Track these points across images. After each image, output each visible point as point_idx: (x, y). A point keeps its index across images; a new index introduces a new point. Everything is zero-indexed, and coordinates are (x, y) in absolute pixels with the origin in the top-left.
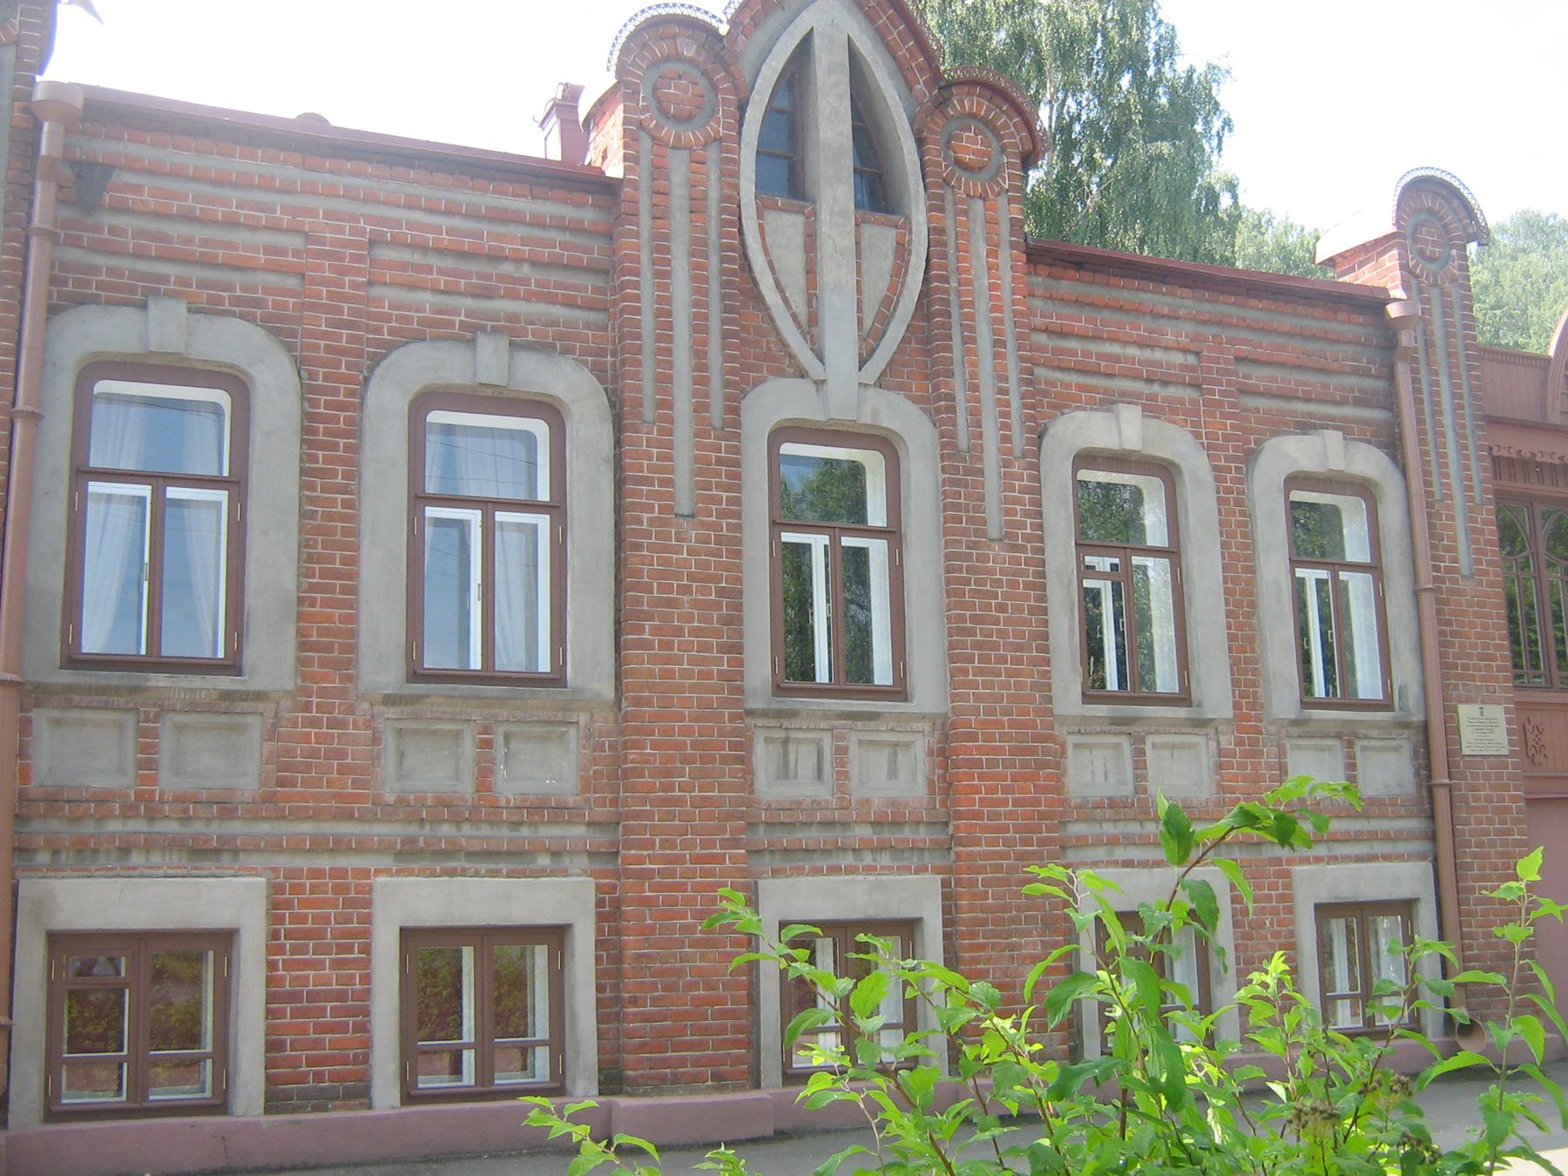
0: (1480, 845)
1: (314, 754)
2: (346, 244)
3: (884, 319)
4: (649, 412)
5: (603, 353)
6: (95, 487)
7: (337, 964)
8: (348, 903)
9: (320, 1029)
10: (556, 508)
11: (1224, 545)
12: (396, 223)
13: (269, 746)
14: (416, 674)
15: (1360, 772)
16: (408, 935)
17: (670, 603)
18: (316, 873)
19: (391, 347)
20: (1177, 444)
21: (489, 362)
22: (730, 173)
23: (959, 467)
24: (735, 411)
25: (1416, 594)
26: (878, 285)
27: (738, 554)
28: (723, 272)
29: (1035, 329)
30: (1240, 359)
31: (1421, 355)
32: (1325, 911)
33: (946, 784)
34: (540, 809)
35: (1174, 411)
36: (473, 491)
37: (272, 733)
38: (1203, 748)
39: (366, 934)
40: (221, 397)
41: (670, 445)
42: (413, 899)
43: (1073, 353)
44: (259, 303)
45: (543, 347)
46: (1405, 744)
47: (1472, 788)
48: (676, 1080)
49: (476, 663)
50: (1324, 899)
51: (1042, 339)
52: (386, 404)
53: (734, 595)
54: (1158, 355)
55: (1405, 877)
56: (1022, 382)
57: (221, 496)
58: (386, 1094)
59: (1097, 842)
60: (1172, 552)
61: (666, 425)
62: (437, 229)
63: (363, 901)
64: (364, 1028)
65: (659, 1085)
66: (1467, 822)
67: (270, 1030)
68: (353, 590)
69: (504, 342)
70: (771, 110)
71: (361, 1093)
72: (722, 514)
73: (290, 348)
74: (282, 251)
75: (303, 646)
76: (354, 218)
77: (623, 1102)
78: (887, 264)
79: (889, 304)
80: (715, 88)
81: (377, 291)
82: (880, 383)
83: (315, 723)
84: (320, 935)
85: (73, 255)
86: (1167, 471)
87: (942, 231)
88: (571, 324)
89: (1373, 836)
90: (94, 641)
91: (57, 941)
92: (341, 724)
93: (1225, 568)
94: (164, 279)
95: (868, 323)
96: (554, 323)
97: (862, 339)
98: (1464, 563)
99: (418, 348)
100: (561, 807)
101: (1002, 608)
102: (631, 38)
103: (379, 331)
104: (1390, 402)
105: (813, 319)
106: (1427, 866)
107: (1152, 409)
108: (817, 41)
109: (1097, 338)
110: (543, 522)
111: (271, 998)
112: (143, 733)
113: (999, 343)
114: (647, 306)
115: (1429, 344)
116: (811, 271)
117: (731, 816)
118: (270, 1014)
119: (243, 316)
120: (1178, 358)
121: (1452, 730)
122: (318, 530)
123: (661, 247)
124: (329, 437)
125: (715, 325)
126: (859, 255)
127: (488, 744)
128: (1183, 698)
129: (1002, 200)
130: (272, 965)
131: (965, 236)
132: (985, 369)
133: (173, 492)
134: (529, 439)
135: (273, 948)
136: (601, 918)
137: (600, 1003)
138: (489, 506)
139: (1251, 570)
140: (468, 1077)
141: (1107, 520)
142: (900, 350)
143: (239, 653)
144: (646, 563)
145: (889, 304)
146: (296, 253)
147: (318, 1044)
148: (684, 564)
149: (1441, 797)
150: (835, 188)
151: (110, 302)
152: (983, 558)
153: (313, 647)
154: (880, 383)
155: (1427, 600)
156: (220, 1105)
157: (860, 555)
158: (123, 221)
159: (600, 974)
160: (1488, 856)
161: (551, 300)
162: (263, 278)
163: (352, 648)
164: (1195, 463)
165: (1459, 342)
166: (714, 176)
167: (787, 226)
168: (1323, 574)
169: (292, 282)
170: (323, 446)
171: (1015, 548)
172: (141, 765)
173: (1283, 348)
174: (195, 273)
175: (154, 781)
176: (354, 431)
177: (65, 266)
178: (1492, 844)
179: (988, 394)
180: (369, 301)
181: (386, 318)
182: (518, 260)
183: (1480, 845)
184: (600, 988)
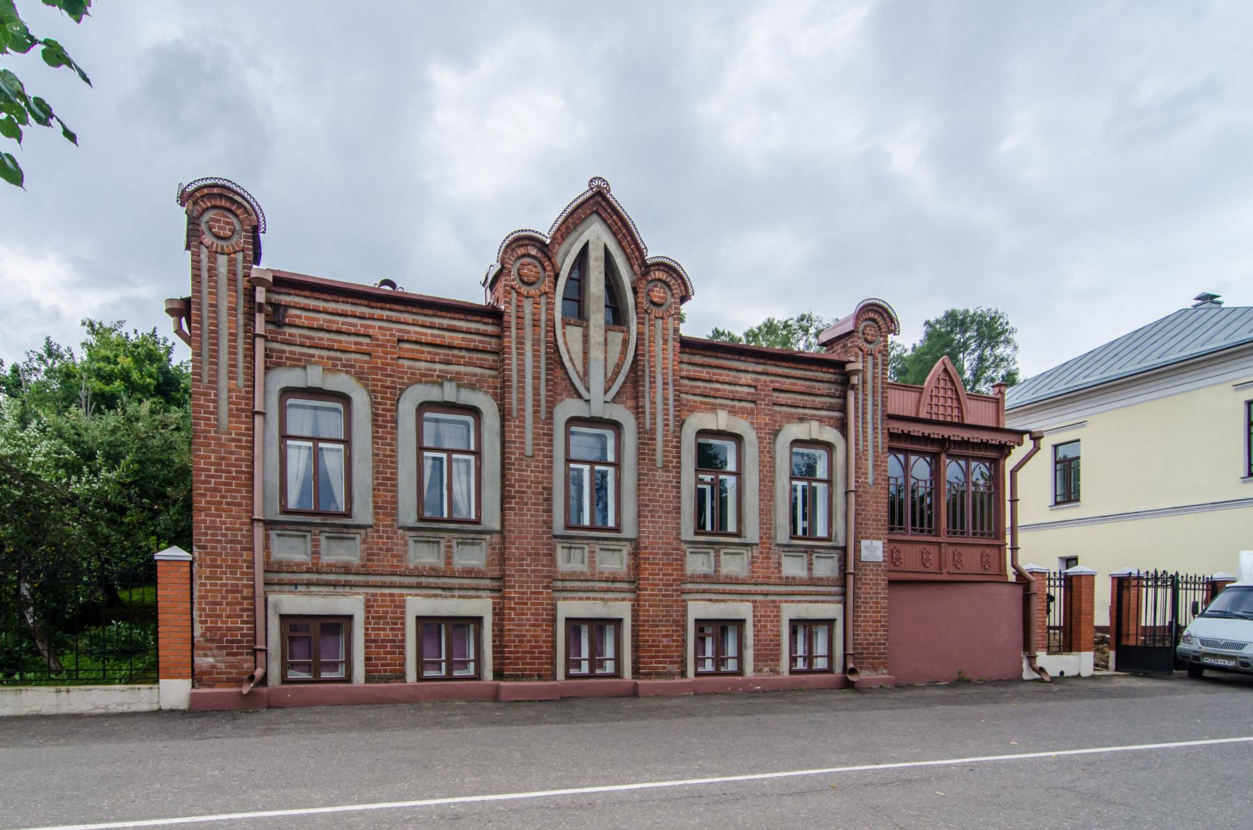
1: (381, 549)
2: (388, 341)
3: (616, 374)
4: (515, 414)
5: (496, 388)
6: (289, 442)
7: (391, 629)
8: (396, 606)
9: (385, 653)
10: (478, 453)
11: (761, 471)
12: (409, 332)
13: (364, 546)
14: (421, 519)
15: (814, 567)
16: (419, 619)
17: (523, 492)
18: (382, 595)
19: (408, 385)
20: (741, 426)
21: (449, 393)
22: (550, 307)
23: (645, 438)
24: (551, 413)
25: (847, 493)
26: (614, 356)
27: (551, 473)
28: (547, 353)
29: (682, 377)
30: (775, 390)
31: (860, 387)
32: (795, 624)
33: (636, 567)
34: (469, 573)
36: (446, 446)
37: (364, 541)
38: (746, 554)
39: (403, 618)
40: (339, 406)
41: (524, 427)
42: (418, 605)
43: (699, 387)
44: (353, 366)
45: (472, 387)
46: (836, 555)
48: (523, 676)
49: (445, 515)
50: (793, 617)
51: (686, 382)
52: (407, 408)
53: (549, 490)
54: (738, 388)
55: (832, 610)
56: (675, 400)
57: (341, 446)
58: (411, 676)
60: (738, 474)
61: (522, 418)
62: (426, 335)
63: (402, 606)
64: (402, 653)
65: (516, 677)
67: (366, 653)
68: (395, 485)
69: (454, 385)
70: (569, 278)
71: (401, 677)
72: (544, 456)
73: (366, 386)
74: (361, 344)
75: (376, 507)
76: (391, 329)
77: (502, 683)
78: (619, 348)
79: (618, 367)
80: (544, 269)
81: (401, 362)
82: (614, 400)
83: (381, 537)
84: (385, 618)
85: (275, 346)
86: (738, 438)
87: (643, 334)
88: (482, 375)
89: (817, 594)
90: (292, 503)
91: (283, 617)
92: (391, 538)
93: (760, 480)
94: (313, 356)
95: (609, 374)
96: (475, 375)
97: (606, 382)
98: (870, 479)
99: (416, 386)
100: (479, 571)
101: (661, 496)
102: (507, 247)
103: (402, 378)
104: (844, 409)
105: (586, 373)
106: (841, 606)
107: (733, 412)
108: (591, 246)
109: (710, 381)
110: (472, 458)
111: (366, 641)
112: (313, 540)
113: (665, 383)
114: (514, 367)
115: (864, 382)
116: (586, 353)
117: (546, 577)
118: (366, 647)
119: (346, 372)
120: (746, 389)
121: (857, 551)
122: (380, 461)
123: (520, 342)
124: (384, 422)
125: (543, 376)
126: (606, 344)
127: (450, 547)
128: (617, 529)
129: (671, 319)
130: (367, 629)
131: (653, 336)
132: (658, 396)
133: (321, 445)
134: (467, 424)
135: (367, 622)
136: (494, 614)
137: (494, 647)
138: (450, 452)
139: (773, 482)
140: (444, 673)
141: (707, 459)
142: (622, 387)
143: (350, 510)
144: (513, 475)
145: (618, 367)
146: (367, 345)
147: (385, 659)
148: (529, 476)
149: (851, 579)
150: (598, 316)
151: (291, 366)
152: (654, 475)
153: (380, 508)
154: (614, 400)
155: (852, 496)
156: (348, 679)
157: (604, 475)
158: (293, 331)
159: (494, 636)
161: (474, 365)
162: (353, 356)
163: (396, 509)
164: (750, 436)
166: (543, 309)
167: (575, 333)
168: (805, 483)
169: (366, 358)
170: (381, 427)
171: (668, 471)
172: (313, 553)
173: (795, 384)
174: (325, 353)
175: (319, 559)
176: (395, 421)
177: (272, 350)
179: (659, 406)
180: (399, 366)
181: (406, 373)
182: (460, 349)
184: (494, 641)
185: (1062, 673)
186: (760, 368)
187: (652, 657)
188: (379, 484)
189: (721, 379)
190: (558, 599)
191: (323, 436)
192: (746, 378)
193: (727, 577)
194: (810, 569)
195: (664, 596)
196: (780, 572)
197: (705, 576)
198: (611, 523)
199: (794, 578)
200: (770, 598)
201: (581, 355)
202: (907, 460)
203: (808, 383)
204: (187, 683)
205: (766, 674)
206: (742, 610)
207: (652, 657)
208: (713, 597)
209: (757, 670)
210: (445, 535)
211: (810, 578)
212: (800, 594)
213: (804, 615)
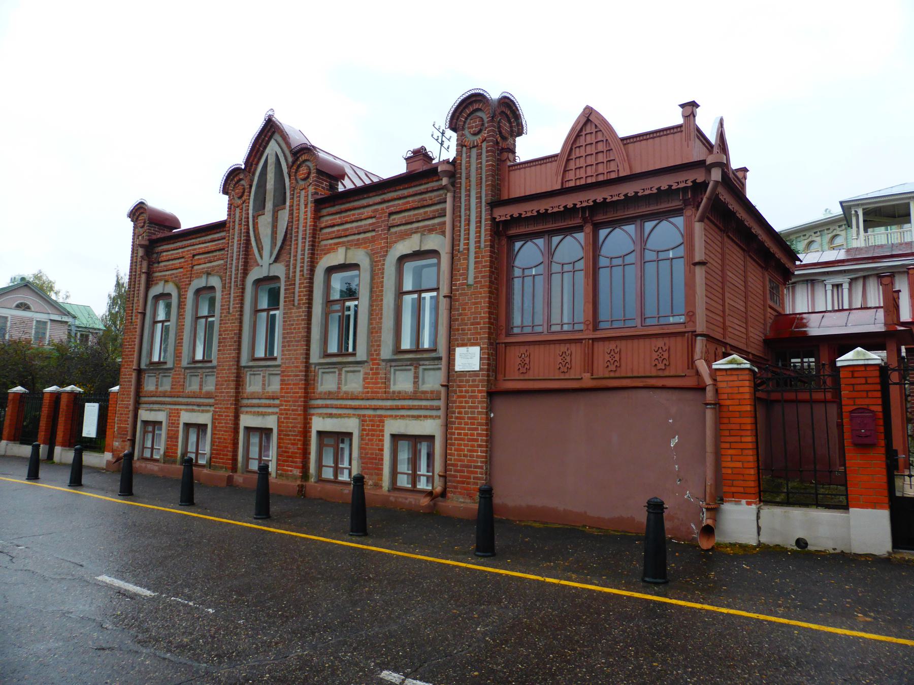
0: (460, 413)
35: (365, 243)
38: (362, 370)
47: (459, 386)
55: (430, 426)
66: (455, 402)
89: (420, 408)
109: (342, 224)
160: (463, 418)
178: (466, 413)
183: (460, 413)
189: (348, 219)
190: (313, 415)
191: (423, 288)
192: (367, 212)
193: (346, 393)
194: (416, 383)
199: (399, 392)
200: (379, 412)
206: (351, 425)
208: (334, 411)
210: (200, 371)
211: (415, 392)
212: (426, 408)
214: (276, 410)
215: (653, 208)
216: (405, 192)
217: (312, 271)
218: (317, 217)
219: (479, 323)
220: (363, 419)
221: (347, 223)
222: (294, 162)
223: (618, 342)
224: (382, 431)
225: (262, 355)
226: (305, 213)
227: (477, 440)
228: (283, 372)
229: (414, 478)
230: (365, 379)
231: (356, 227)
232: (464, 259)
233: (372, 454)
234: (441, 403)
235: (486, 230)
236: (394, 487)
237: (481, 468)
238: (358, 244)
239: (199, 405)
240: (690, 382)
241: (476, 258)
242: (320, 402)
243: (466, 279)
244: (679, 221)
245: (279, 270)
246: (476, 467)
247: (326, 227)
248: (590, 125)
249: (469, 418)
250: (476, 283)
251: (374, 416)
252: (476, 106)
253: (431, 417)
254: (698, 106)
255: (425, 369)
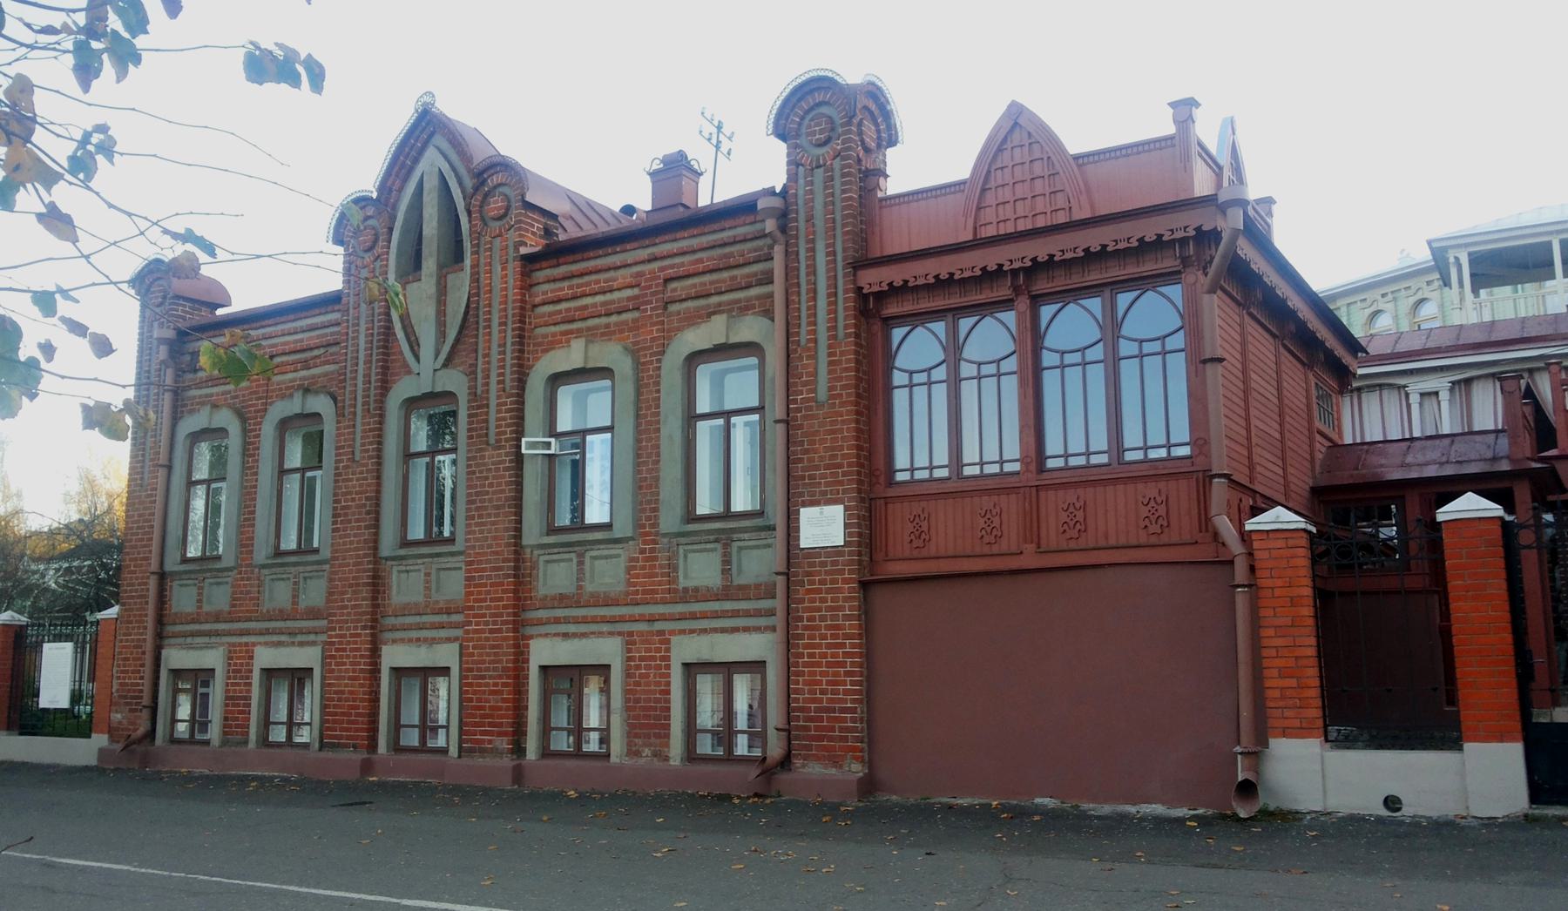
35: (621, 331)
59: (548, 622)
89: (735, 614)
154: (445, 365)
164: (234, 428)
165: (462, 171)
185: (1392, 803)
186: (644, 254)
187: (476, 724)
188: (650, 486)
192: (623, 276)
193: (592, 595)
194: (726, 572)
195: (491, 631)
196: (675, 580)
197: (562, 597)
198: (446, 534)
199: (696, 590)
200: (658, 626)
201: (431, 311)
202: (953, 332)
203: (719, 251)
204: (106, 737)
205: (646, 759)
206: (608, 649)
207: (476, 724)
208: (572, 628)
209: (633, 752)
211: (726, 588)
213: (706, 655)
214: (459, 633)
215: (1131, 270)
216: (695, 242)
217: (521, 383)
218: (527, 286)
219: (840, 466)
220: (629, 640)
221: (584, 295)
222: (476, 189)
223: (1080, 491)
224: (667, 658)
225: (293, 546)
226: (503, 280)
227: (843, 665)
228: (470, 563)
229: (291, 725)
230: (629, 570)
231: (604, 304)
232: (809, 357)
233: (649, 700)
234: (778, 603)
235: (846, 309)
236: (691, 756)
237: (853, 710)
238: (607, 334)
239: (292, 633)
240: (1205, 553)
241: (830, 355)
242: (542, 614)
243: (814, 391)
244: (1175, 291)
245: (454, 381)
246: (844, 710)
247: (544, 304)
248: (1018, 137)
249: (828, 627)
250: (832, 397)
251: (651, 633)
252: (819, 97)
253: (746, 629)
254: (1197, 105)
255: (740, 548)
